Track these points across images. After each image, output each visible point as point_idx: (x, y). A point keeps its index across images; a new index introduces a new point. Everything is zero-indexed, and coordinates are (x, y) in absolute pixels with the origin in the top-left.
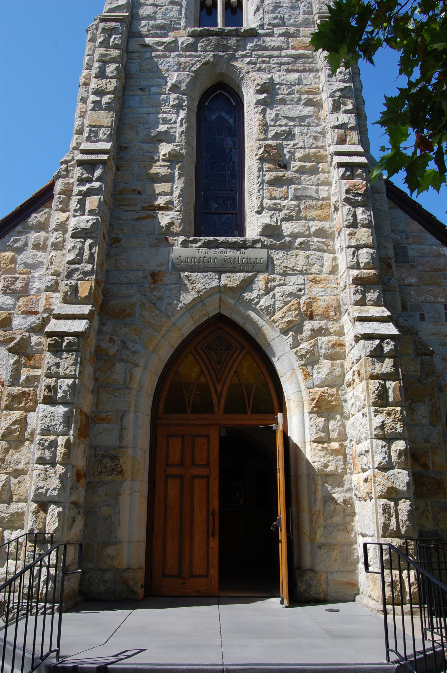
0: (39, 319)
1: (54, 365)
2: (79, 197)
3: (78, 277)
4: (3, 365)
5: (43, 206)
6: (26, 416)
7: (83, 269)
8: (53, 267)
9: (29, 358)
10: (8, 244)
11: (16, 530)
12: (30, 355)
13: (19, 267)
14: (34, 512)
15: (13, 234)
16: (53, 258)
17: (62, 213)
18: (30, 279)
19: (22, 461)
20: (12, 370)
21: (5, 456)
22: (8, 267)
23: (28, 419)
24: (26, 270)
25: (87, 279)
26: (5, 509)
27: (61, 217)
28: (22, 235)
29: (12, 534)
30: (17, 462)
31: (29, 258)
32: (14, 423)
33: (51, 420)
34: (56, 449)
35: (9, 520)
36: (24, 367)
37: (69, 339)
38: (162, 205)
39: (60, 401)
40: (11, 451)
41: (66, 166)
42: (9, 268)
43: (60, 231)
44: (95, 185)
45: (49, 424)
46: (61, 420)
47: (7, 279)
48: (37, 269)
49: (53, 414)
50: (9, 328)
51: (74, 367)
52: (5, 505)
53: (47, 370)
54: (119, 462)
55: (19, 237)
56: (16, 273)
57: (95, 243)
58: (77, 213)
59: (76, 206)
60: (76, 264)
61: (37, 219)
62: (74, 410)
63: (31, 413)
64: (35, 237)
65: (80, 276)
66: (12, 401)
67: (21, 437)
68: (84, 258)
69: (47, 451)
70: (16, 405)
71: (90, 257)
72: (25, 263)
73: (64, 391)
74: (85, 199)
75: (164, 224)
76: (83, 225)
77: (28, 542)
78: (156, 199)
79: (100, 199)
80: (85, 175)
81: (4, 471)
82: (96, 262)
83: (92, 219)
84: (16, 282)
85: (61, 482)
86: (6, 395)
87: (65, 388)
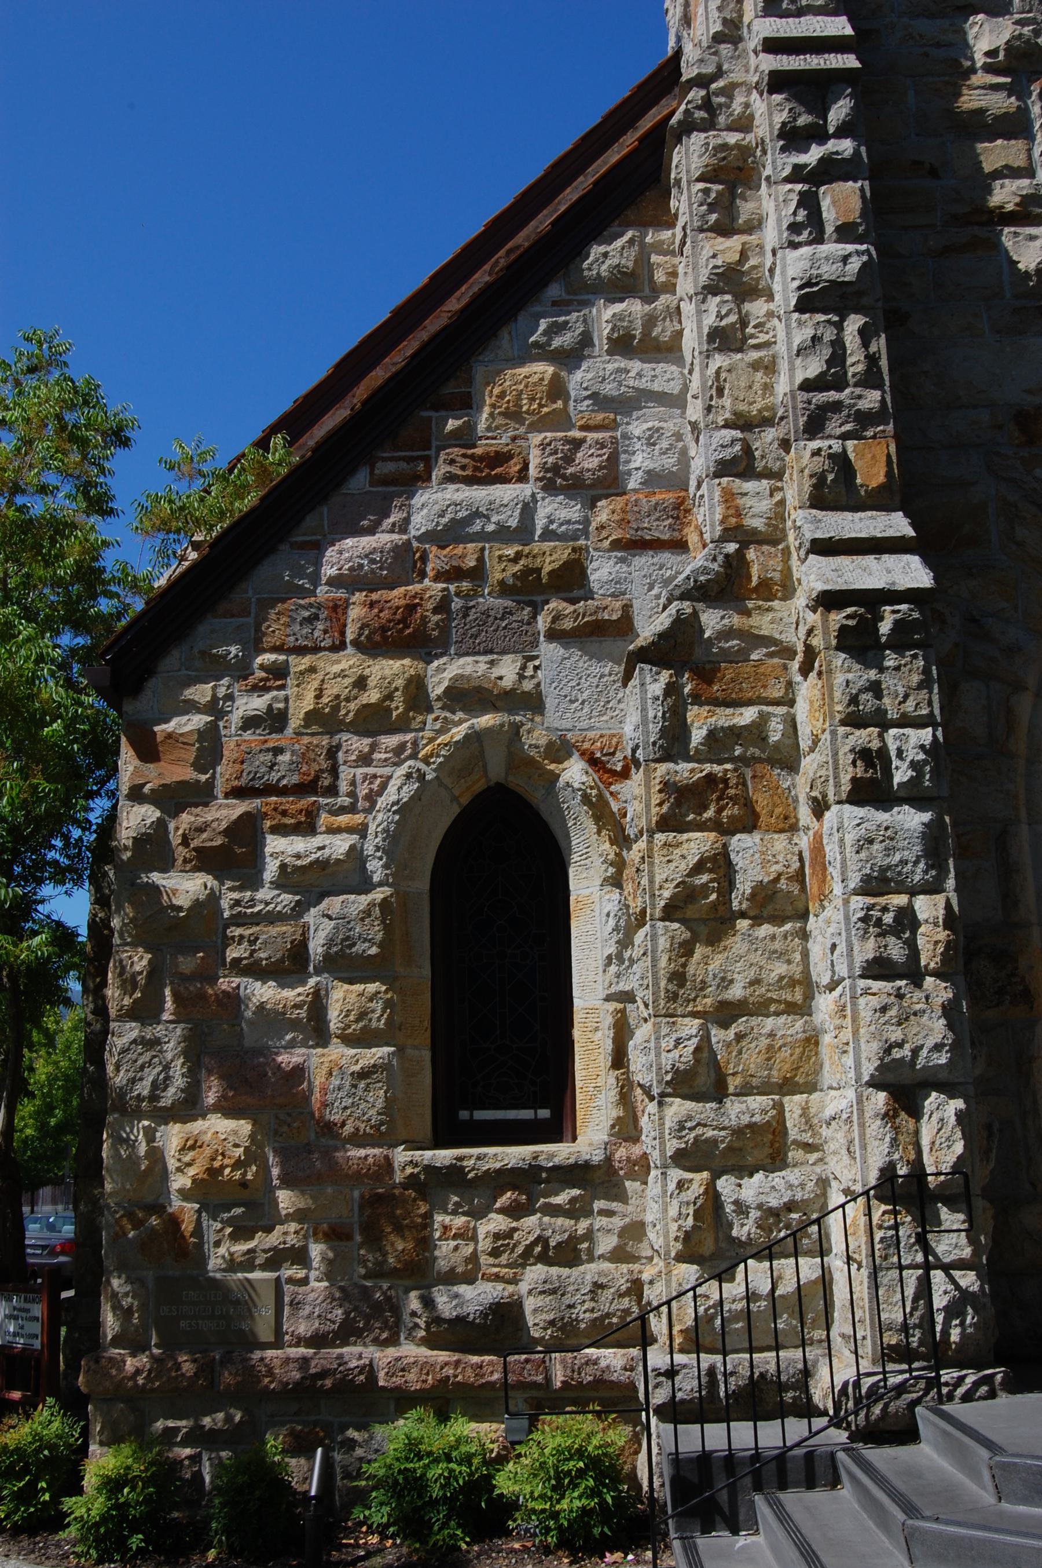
0: (714, 559)
1: (866, 690)
2: (799, 187)
3: (844, 429)
4: (583, 703)
5: (617, 222)
6: (725, 846)
7: (855, 405)
8: (727, 401)
9: (706, 674)
10: (532, 339)
11: (751, 1176)
12: (707, 666)
13: (580, 409)
14: (886, 1115)
15: (539, 309)
16: (723, 375)
17: (720, 240)
18: (617, 443)
19: (736, 976)
20: (664, 713)
21: (684, 965)
22: (545, 410)
23: (732, 856)
24: (600, 416)
25: (869, 433)
26: (712, 1115)
27: (723, 252)
28: (569, 313)
29: (740, 1185)
30: (723, 979)
31: (604, 379)
32: (698, 868)
33: (889, 851)
34: (914, 933)
35: (730, 1148)
36: (692, 704)
37: (898, 611)
38: (1010, 207)
39: (902, 794)
40: (700, 951)
41: (703, 93)
42: (548, 413)
43: (726, 293)
44: (840, 148)
45: (881, 861)
46: (918, 848)
47: (549, 444)
48: (635, 414)
49: (889, 833)
50: (581, 592)
51: (924, 694)
52: (708, 1105)
53: (849, 705)
54: (1017, 968)
55: (563, 318)
56: (570, 426)
57: (874, 324)
58: (799, 234)
59: (795, 214)
60: (827, 388)
61: (608, 262)
62: (947, 819)
63: (738, 836)
64: (614, 315)
65: (848, 427)
66: (678, 803)
67: (721, 908)
68: (851, 371)
69: (892, 940)
70: (691, 817)
71: (868, 370)
72: (594, 396)
73: (913, 765)
74: (816, 193)
75: (1032, 266)
76: (829, 271)
77: (874, 1202)
78: (989, 191)
79: (862, 189)
80: (803, 120)
81: (689, 1009)
82: (887, 383)
83: (858, 253)
84: (579, 455)
85: (950, 1026)
86: (658, 788)
87: (914, 754)
